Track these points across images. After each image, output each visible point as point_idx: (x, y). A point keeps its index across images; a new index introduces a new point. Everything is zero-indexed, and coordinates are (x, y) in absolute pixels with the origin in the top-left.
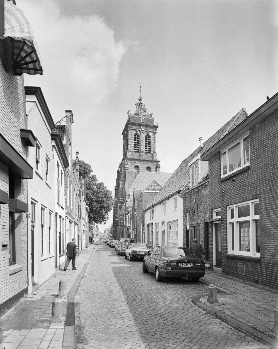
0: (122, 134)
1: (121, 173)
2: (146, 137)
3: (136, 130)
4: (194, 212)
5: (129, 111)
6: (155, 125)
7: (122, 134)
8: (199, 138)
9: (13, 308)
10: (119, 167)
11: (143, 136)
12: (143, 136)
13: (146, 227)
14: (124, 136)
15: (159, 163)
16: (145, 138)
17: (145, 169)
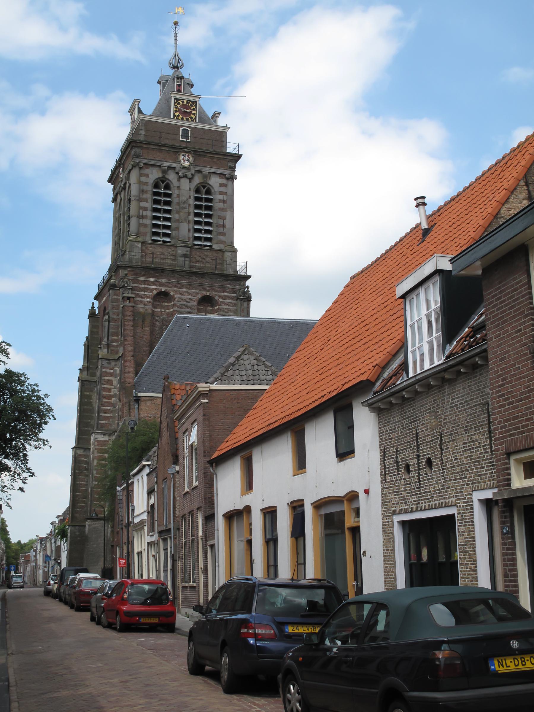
0: (110, 181)
1: (106, 317)
2: (197, 191)
3: (160, 166)
4: (429, 462)
5: (135, 101)
6: (229, 150)
7: (110, 181)
8: (416, 199)
9: (172, 641)
10: (96, 298)
11: (183, 190)
12: (183, 190)
13: (220, 523)
14: (114, 189)
15: (248, 283)
16: (193, 194)
17: (195, 304)
